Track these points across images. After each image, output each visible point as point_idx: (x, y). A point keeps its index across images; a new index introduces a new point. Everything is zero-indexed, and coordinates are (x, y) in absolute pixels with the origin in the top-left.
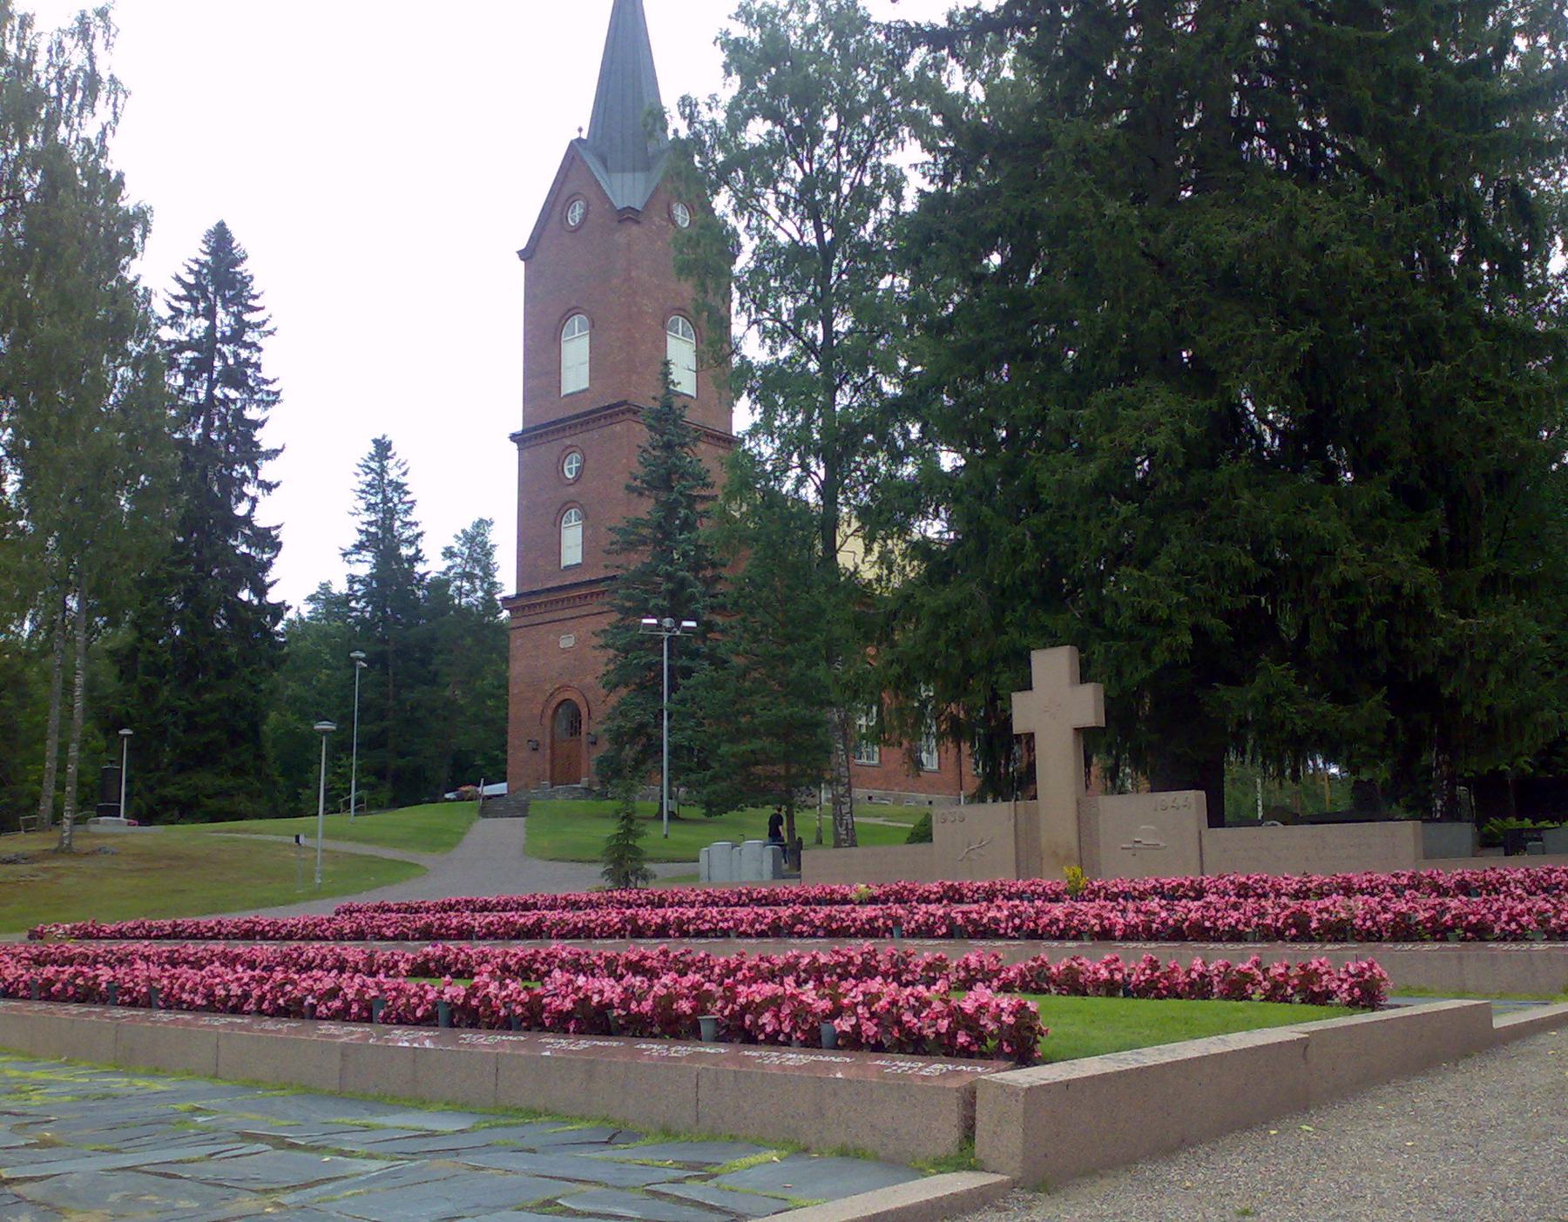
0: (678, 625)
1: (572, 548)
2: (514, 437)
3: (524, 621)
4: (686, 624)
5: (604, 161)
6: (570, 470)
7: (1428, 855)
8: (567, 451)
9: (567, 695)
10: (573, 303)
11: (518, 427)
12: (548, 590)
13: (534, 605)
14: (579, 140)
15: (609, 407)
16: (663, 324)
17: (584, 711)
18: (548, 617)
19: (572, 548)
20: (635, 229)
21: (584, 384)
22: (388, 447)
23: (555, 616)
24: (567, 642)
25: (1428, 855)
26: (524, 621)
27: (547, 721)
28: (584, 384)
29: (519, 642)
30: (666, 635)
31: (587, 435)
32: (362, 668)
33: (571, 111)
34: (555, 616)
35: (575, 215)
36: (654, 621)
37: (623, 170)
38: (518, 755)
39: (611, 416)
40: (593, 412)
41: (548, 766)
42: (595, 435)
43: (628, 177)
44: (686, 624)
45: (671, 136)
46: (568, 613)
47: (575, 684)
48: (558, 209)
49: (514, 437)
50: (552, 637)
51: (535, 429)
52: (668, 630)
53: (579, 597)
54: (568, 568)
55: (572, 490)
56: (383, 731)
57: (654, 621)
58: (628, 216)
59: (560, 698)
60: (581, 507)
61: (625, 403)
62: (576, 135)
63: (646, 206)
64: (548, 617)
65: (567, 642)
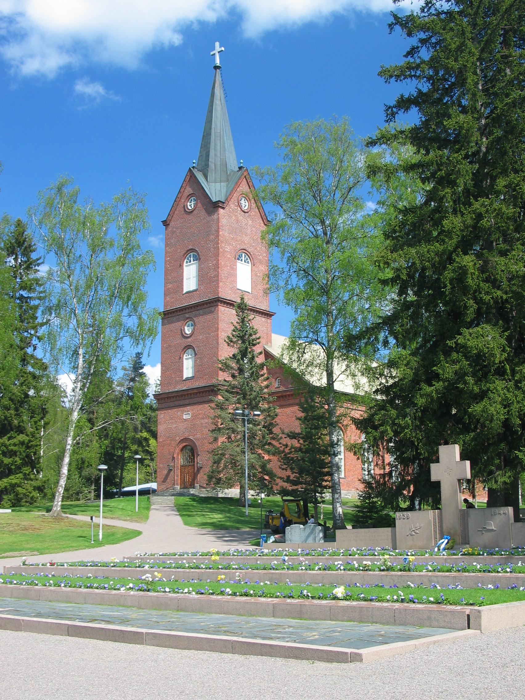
1: (188, 368)
19: (188, 368)
20: (221, 211)
26: (164, 405)
54: (188, 379)
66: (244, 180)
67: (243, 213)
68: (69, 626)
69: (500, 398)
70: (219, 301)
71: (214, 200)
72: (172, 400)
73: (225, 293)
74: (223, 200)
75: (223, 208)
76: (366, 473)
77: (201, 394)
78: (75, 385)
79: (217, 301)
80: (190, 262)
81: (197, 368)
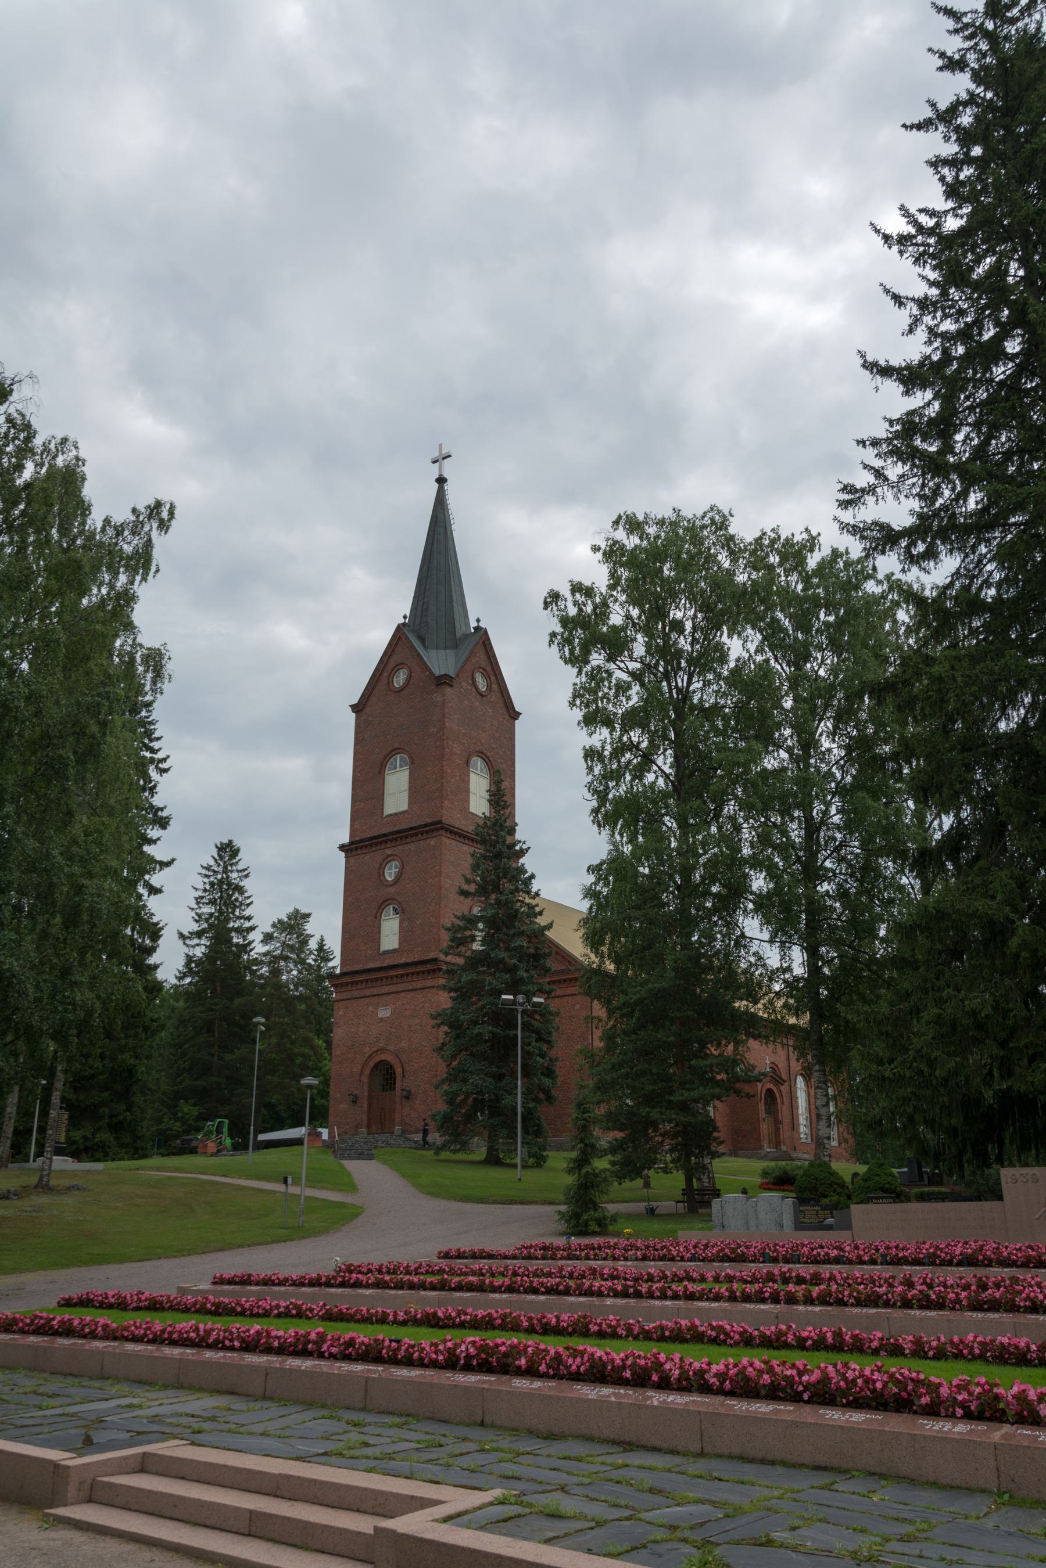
0: (529, 1000)
1: (390, 933)
2: (342, 848)
3: (345, 995)
4: (535, 999)
5: (422, 640)
6: (390, 873)
7: (800, 1226)
8: (388, 859)
9: (384, 1057)
10: (397, 745)
11: (346, 839)
12: (369, 971)
13: (357, 982)
14: (404, 624)
15: (426, 825)
16: (467, 763)
17: (398, 1071)
18: (368, 992)
19: (390, 933)
20: (449, 690)
21: (404, 806)
22: (235, 853)
23: (375, 991)
24: (384, 1013)
25: (800, 1226)
26: (345, 995)
27: (365, 1079)
28: (404, 806)
29: (341, 1012)
30: (520, 1009)
31: (406, 847)
32: (262, 1032)
34: (375, 991)
35: (400, 679)
36: (511, 997)
37: (437, 648)
38: (338, 1105)
40: (412, 829)
41: (365, 1117)
42: (413, 847)
43: (442, 652)
44: (535, 999)
46: (385, 989)
47: (391, 1048)
48: (386, 674)
49: (342, 848)
50: (371, 1008)
51: (361, 841)
52: (522, 1004)
53: (397, 976)
54: (386, 952)
55: (391, 890)
57: (511, 997)
59: (377, 1059)
61: (440, 822)
62: (402, 621)
64: (368, 992)
65: (384, 1013)
66: (482, 647)
67: (479, 696)
68: (253, 1515)
69: (753, 950)
70: (442, 828)
71: (437, 673)
72: (359, 986)
73: (451, 817)
74: (452, 674)
75: (451, 686)
76: (647, 953)
77: (410, 978)
78: (78, 858)
79: (436, 827)
80: (395, 768)
81: (405, 934)
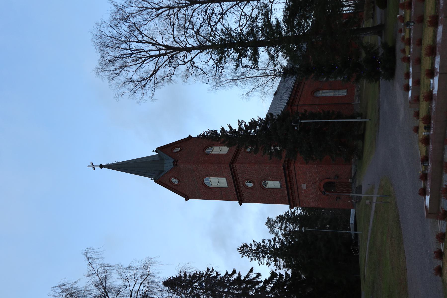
1: (274, 184)
8: (245, 186)
9: (322, 187)
10: (200, 182)
12: (288, 192)
17: (327, 180)
19: (274, 184)
23: (296, 191)
24: (304, 186)
33: (147, 183)
35: (175, 181)
39: (234, 170)
42: (240, 176)
45: (264, 270)
46: (295, 186)
48: (173, 187)
49: (240, 204)
55: (256, 184)
56: (281, 158)
58: (175, 163)
60: (262, 181)
63: (173, 158)
65: (304, 186)
